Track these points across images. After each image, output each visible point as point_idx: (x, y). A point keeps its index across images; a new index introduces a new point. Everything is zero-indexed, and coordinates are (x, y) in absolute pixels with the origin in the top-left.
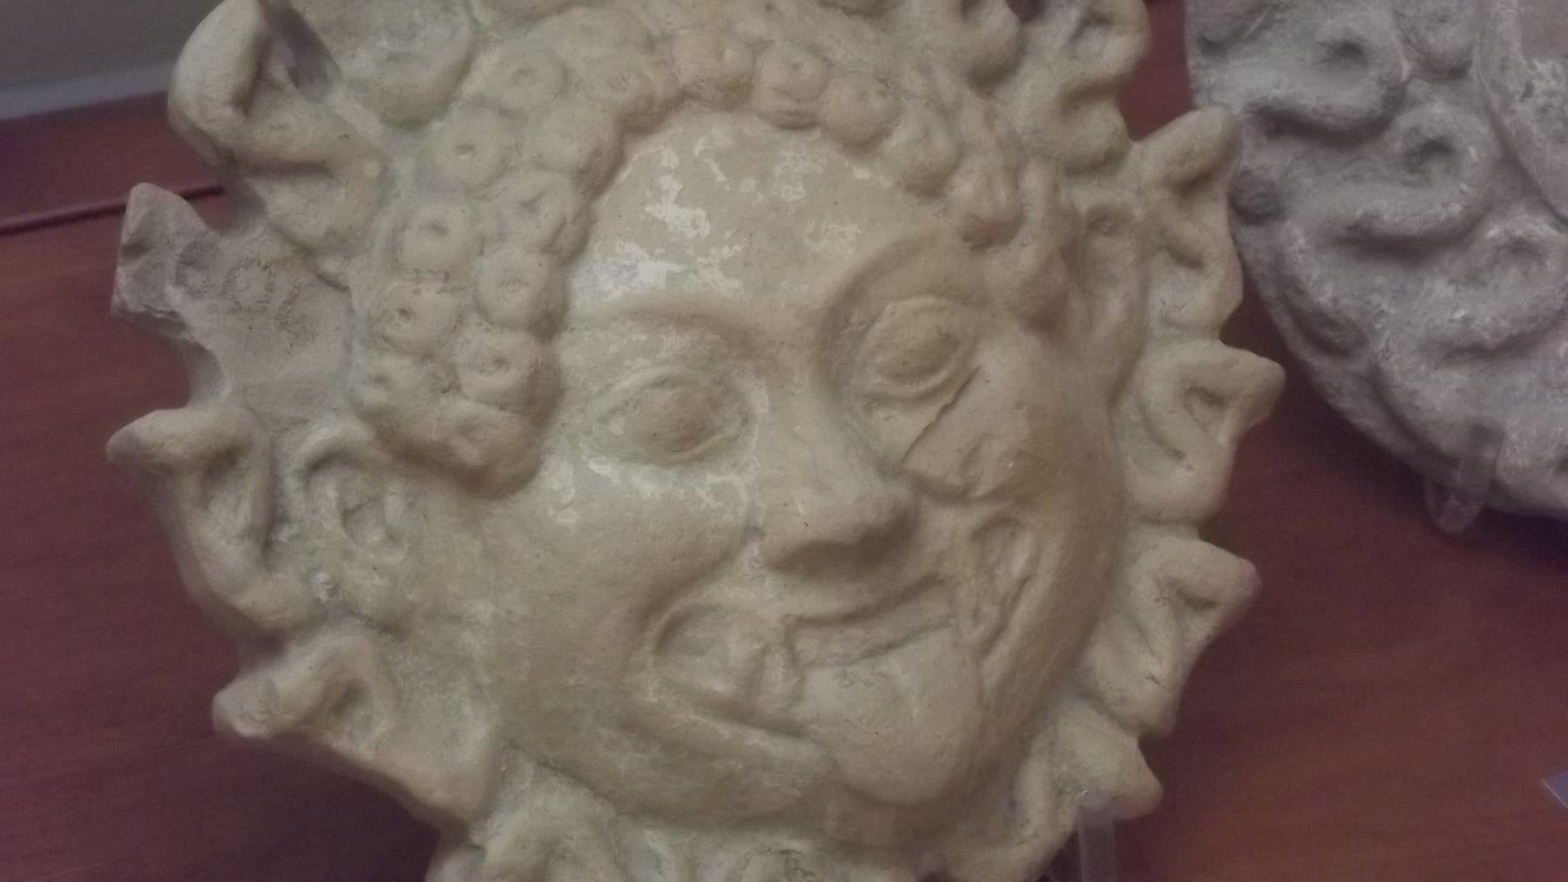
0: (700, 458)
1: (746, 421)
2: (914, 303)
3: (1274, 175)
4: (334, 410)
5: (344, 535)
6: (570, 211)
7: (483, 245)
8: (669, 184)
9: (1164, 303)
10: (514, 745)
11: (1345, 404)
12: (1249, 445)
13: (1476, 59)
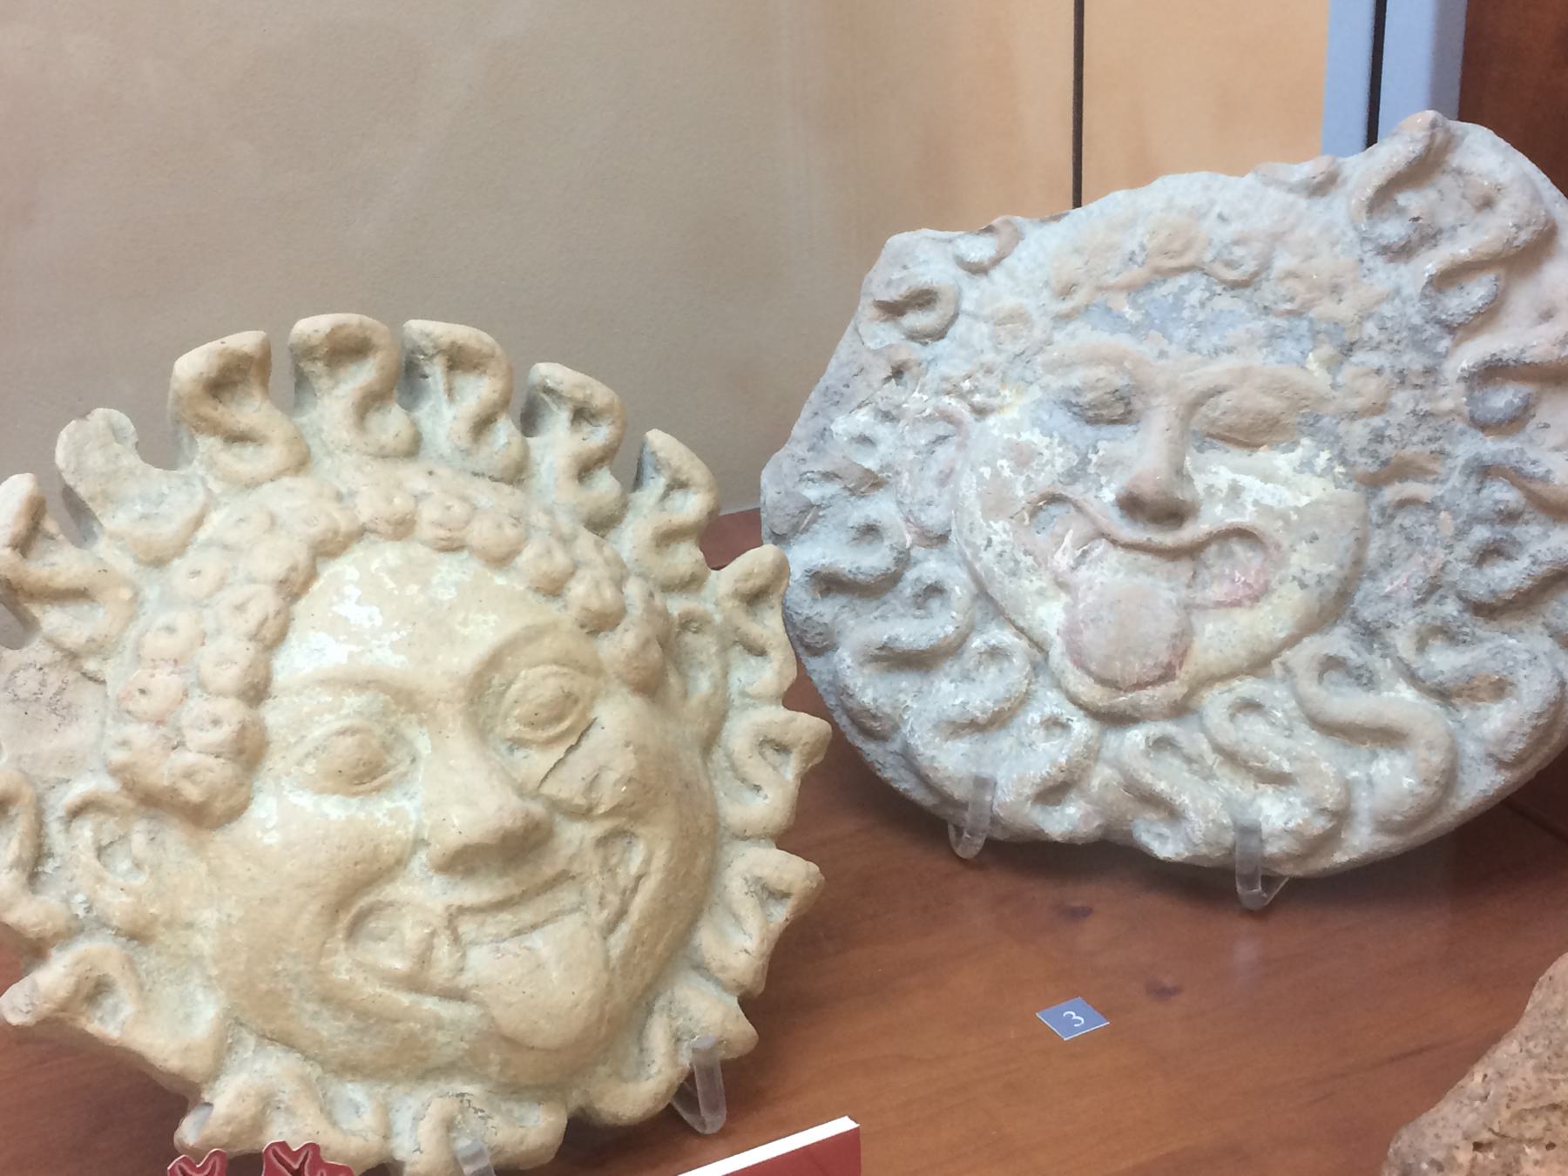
0: (378, 789)
1: (413, 760)
2: (541, 670)
3: (827, 619)
4: (91, 771)
5: (98, 864)
6: (272, 610)
7: (204, 638)
8: (352, 591)
9: (740, 681)
10: (239, 1023)
11: (888, 774)
12: (809, 781)
13: (954, 528)
